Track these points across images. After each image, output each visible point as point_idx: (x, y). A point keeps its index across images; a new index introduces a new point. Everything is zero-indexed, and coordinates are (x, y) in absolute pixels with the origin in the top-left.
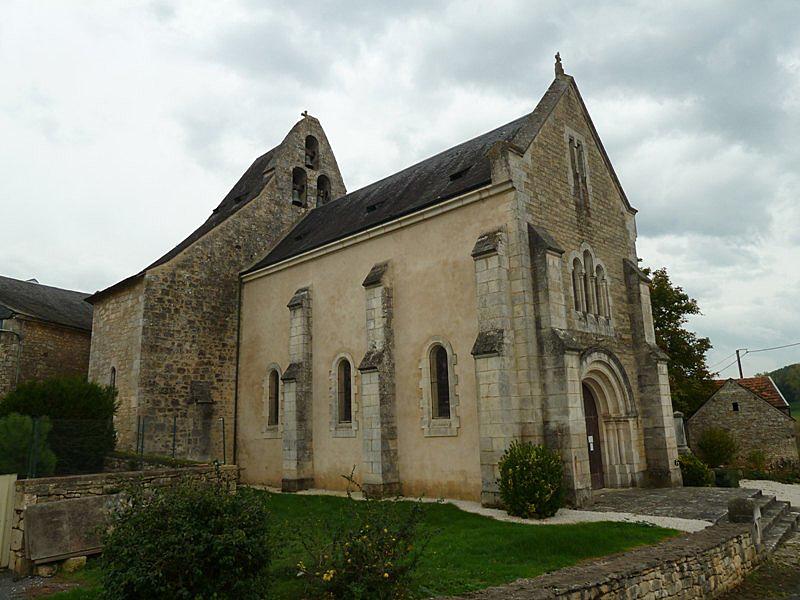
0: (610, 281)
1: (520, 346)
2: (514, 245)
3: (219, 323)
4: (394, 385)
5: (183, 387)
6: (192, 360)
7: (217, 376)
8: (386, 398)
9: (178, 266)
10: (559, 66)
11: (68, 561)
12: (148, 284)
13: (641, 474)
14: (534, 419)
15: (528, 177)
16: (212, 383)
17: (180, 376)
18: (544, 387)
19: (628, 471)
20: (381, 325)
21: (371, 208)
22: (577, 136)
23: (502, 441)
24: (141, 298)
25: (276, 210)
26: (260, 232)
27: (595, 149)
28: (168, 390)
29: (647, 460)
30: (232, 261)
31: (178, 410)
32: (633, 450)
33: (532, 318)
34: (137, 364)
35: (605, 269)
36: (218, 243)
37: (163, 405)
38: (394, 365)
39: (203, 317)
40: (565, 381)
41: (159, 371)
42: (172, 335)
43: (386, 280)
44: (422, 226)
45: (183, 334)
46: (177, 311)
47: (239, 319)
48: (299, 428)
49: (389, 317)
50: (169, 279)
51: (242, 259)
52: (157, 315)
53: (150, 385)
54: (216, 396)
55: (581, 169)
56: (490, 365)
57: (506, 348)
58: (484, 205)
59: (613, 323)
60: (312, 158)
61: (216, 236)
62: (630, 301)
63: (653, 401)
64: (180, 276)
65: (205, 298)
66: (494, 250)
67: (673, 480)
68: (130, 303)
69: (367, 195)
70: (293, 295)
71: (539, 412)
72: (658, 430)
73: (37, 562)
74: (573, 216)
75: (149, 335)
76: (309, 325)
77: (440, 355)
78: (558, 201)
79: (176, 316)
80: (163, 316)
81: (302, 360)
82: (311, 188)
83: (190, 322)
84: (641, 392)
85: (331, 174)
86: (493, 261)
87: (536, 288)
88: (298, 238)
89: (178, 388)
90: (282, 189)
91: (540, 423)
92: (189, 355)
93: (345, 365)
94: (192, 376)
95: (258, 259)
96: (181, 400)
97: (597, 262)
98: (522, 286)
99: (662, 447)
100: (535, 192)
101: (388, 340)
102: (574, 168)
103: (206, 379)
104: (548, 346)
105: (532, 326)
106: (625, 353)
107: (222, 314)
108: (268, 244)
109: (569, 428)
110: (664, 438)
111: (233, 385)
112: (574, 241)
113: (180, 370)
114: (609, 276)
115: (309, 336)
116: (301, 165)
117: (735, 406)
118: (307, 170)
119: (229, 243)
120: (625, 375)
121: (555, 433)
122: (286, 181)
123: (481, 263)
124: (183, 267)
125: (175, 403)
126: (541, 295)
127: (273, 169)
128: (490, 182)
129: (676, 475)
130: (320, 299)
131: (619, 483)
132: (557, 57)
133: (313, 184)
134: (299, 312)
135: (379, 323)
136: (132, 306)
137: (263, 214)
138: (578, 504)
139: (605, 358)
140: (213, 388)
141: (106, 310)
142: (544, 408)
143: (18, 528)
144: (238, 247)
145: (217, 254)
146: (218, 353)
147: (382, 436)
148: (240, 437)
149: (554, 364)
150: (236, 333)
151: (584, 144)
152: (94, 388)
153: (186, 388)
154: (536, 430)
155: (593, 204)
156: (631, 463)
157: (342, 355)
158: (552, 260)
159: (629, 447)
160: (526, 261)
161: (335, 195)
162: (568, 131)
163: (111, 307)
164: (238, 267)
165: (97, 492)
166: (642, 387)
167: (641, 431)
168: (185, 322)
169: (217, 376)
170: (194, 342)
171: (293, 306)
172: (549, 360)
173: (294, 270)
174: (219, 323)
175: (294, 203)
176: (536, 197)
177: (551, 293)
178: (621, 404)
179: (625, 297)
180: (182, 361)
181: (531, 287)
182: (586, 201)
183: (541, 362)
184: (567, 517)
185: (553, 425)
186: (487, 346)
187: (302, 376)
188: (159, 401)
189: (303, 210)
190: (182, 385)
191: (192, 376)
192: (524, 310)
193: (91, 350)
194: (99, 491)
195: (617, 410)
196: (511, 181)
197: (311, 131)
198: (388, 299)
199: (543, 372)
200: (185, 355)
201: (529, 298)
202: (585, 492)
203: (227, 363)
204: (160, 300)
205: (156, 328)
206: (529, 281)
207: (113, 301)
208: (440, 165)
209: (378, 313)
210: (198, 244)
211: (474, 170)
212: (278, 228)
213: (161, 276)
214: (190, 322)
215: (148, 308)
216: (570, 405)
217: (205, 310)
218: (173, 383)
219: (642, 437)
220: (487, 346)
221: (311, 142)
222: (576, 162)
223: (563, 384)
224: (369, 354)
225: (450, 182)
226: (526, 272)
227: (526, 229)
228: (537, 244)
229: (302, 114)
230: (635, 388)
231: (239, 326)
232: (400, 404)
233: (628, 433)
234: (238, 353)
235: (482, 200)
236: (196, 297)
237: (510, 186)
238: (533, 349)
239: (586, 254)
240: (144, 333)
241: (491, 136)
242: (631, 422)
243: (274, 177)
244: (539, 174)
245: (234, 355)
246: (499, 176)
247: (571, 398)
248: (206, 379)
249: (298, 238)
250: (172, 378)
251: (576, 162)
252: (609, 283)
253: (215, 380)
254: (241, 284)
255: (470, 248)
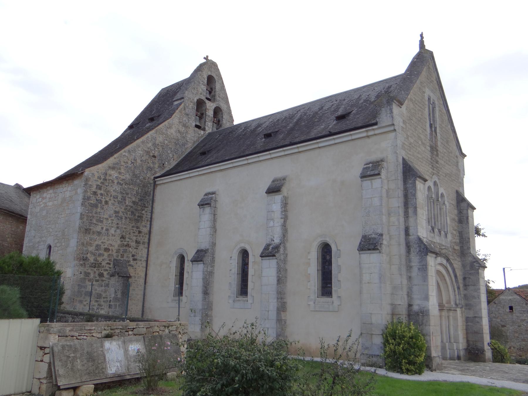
0: (449, 204)
1: (393, 245)
2: (392, 172)
3: (137, 214)
4: (286, 270)
5: (108, 263)
6: (116, 243)
7: (133, 256)
8: (281, 280)
9: (109, 167)
10: (422, 44)
11: (81, 388)
12: (87, 180)
13: (464, 351)
14: (402, 302)
15: (404, 123)
16: (129, 261)
17: (106, 254)
18: (410, 278)
19: (455, 348)
20: (280, 224)
21: (268, 136)
22: (432, 95)
23: (381, 318)
24: (80, 191)
25: (180, 130)
26: (170, 146)
27: (442, 107)
28: (96, 265)
29: (468, 341)
30: (149, 167)
31: (103, 281)
32: (460, 333)
33: (402, 227)
34: (73, 243)
35: (445, 197)
36: (140, 152)
37: (92, 276)
38: (287, 255)
39: (125, 209)
40: (427, 275)
41: (91, 249)
42: (102, 222)
43: (284, 190)
44: (317, 151)
45: (110, 222)
46: (106, 202)
47: (152, 213)
48: (204, 299)
49: (285, 218)
50: (102, 177)
51: (157, 166)
52: (92, 204)
53: (83, 260)
54: (131, 271)
55: (434, 121)
56: (371, 259)
57: (384, 248)
58: (368, 140)
59: (449, 236)
60: (210, 93)
61: (139, 146)
62: (460, 221)
63: (474, 297)
64: (110, 175)
65: (127, 194)
66: (379, 174)
67: (487, 358)
68: (68, 194)
69: (259, 125)
70: (202, 196)
71: (406, 297)
72: (477, 319)
73: (61, 387)
74: (428, 155)
75: (85, 219)
76: (215, 221)
77: (326, 252)
78: (420, 143)
79: (106, 207)
80: (96, 206)
81: (207, 248)
82: (209, 116)
83: (116, 212)
84: (465, 290)
85: (223, 106)
86: (377, 182)
87: (406, 205)
88: (203, 153)
89: (104, 263)
90: (188, 115)
91: (406, 306)
92: (113, 238)
93: (182, 259)
94: (115, 254)
95: (168, 167)
96: (105, 273)
97: (441, 190)
98: (397, 202)
99: (479, 333)
100: (407, 135)
101: (284, 236)
102: (430, 119)
103: (125, 258)
104: (415, 249)
105: (403, 233)
106: (456, 260)
107: (139, 208)
108: (175, 157)
109: (429, 310)
110: (482, 325)
111: (144, 264)
112: (428, 173)
113: (107, 250)
114: (448, 202)
115: (214, 228)
116: (203, 98)
117: (511, 308)
118: (207, 101)
119: (148, 153)
120: (456, 276)
121: (417, 314)
122: (191, 107)
123: (367, 183)
124: (113, 168)
125: (101, 275)
126: (411, 211)
127: (183, 98)
128: (376, 124)
129: (489, 354)
130: (224, 201)
131: (448, 356)
132: (421, 36)
133: (210, 113)
134: (207, 210)
135: (278, 222)
136: (71, 197)
137: (174, 133)
138: (434, 368)
139: (444, 262)
140: (130, 265)
141: (43, 198)
142: (409, 295)
143: (42, 361)
144: (154, 156)
145: (139, 161)
146: (134, 238)
147: (277, 308)
148: (147, 305)
149: (420, 262)
150: (149, 223)
151: (436, 102)
152: (35, 261)
153: (110, 264)
154: (403, 311)
155: (440, 148)
156: (457, 342)
157: (242, 245)
158: (419, 185)
159: (456, 330)
160: (400, 183)
161: (226, 124)
162: (428, 92)
163: (48, 196)
164: (153, 172)
165: (98, 336)
166: (466, 286)
167: (464, 319)
168: (112, 212)
169: (133, 256)
170: (118, 228)
171: (203, 204)
172: (415, 260)
173: (203, 177)
174: (137, 214)
175: (197, 126)
176: (408, 138)
177: (418, 210)
178: (452, 297)
179: (456, 218)
180: (109, 242)
181: (403, 204)
182: (437, 146)
183: (409, 260)
184: (427, 376)
185: (415, 308)
186: (369, 244)
187: (208, 259)
188: (89, 273)
189: (202, 132)
190: (106, 262)
191: (115, 254)
192: (398, 220)
193: (27, 230)
194: (99, 335)
195: (449, 302)
196: (393, 125)
197: (211, 71)
198: (285, 204)
199: (409, 268)
200: (110, 238)
201: (401, 211)
202: (437, 359)
203: (141, 246)
204: (95, 193)
205: (91, 215)
206: (402, 200)
207: (51, 191)
208: (322, 108)
209: (277, 214)
210: (125, 152)
211: (355, 114)
212: (184, 145)
213: (97, 175)
214: (116, 212)
215: (86, 199)
216: (430, 294)
217: (127, 203)
218: (100, 259)
219: (465, 324)
220: (369, 244)
221: (211, 80)
222: (431, 115)
223: (425, 278)
224: (268, 245)
225: (335, 122)
226: (400, 193)
227: (401, 160)
228: (409, 173)
229: (205, 58)
230: (461, 286)
231: (151, 218)
232: (291, 286)
233: (456, 319)
234: (149, 240)
235: (368, 137)
236: (121, 193)
237: (392, 128)
238: (403, 249)
239: (435, 183)
240: (81, 218)
241: (364, 90)
242: (459, 310)
243: (183, 105)
244: (394, 121)
245: (146, 240)
246: (384, 119)
247: (430, 288)
248: (125, 258)
249: (203, 153)
250: (100, 255)
251: (431, 115)
252: (448, 207)
253: (131, 259)
254: (155, 185)
255: (358, 171)
